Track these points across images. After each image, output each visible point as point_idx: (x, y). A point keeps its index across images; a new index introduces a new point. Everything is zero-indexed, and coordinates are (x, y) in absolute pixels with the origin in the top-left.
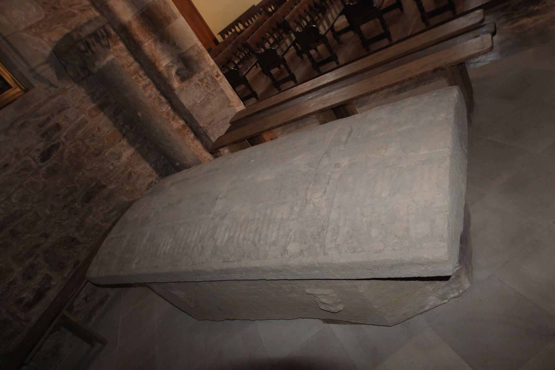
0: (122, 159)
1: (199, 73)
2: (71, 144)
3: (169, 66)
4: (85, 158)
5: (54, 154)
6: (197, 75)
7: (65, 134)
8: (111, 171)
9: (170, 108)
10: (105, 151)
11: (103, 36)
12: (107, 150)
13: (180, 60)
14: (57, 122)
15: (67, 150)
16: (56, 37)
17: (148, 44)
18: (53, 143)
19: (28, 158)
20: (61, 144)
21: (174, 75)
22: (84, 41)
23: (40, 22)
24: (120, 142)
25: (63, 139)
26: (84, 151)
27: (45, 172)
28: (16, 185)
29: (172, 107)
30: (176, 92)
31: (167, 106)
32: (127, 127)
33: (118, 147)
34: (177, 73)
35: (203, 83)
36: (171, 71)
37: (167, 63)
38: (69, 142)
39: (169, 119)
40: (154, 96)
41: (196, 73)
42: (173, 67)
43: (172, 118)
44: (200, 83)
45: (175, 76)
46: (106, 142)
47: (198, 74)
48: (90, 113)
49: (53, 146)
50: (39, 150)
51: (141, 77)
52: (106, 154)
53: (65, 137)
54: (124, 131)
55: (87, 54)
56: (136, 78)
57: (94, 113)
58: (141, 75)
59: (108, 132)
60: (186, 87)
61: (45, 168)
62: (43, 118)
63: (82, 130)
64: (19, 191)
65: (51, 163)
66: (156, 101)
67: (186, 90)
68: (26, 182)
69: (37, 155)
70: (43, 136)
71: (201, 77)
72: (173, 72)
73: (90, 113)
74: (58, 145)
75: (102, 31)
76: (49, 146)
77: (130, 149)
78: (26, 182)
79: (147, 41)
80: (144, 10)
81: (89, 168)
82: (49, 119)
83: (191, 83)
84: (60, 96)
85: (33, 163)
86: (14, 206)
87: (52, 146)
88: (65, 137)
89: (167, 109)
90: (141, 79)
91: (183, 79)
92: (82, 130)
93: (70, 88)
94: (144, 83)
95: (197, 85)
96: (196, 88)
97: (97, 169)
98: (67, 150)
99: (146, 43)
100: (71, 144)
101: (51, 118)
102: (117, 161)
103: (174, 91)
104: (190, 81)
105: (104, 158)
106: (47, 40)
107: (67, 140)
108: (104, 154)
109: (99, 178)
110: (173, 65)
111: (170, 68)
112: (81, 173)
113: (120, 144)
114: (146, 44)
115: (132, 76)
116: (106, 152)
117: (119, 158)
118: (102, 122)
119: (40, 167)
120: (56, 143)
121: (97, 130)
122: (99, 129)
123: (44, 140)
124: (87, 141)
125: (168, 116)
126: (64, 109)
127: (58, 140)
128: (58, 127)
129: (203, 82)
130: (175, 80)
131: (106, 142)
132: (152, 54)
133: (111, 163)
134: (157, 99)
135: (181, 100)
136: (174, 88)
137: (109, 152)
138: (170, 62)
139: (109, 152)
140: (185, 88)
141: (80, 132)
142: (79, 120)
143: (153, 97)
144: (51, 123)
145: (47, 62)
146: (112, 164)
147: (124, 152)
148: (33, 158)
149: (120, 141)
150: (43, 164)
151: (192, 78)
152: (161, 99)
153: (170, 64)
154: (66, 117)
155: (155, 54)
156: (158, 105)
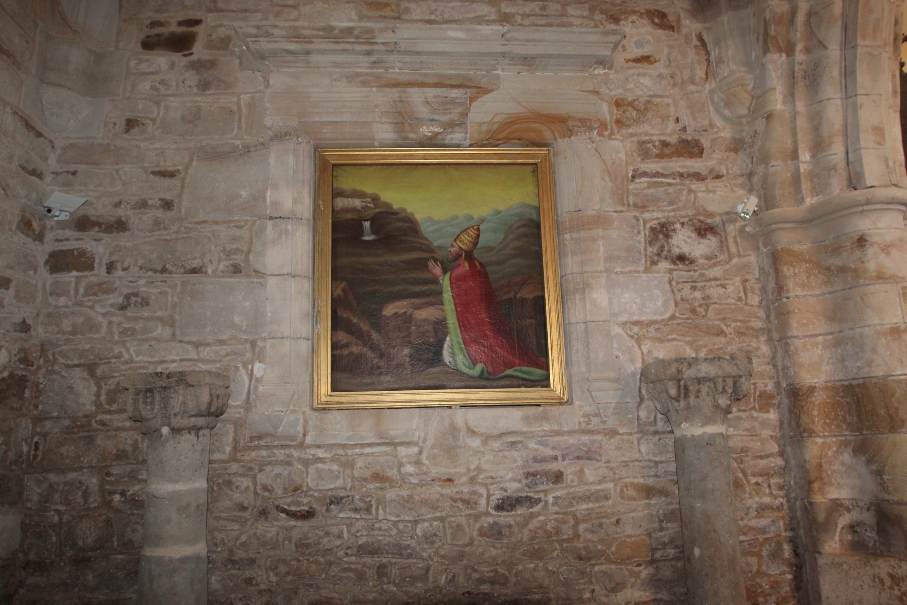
0: (616, 595)
1: (901, 560)
2: (557, 513)
3: (841, 505)
4: (558, 547)
5: (520, 511)
6: (893, 562)
7: (559, 493)
8: (580, 599)
9: (790, 577)
10: (599, 562)
11: (724, 391)
12: (604, 562)
13: (872, 508)
14: (562, 469)
15: (542, 518)
16: (662, 352)
17: (824, 443)
18: (531, 494)
19: (483, 491)
20: (543, 503)
21: (840, 526)
22: (682, 383)
23: (656, 322)
24: (636, 566)
25: (550, 499)
26: (566, 537)
27: (486, 525)
28: (438, 514)
29: (795, 578)
30: (821, 561)
31: (786, 569)
32: (671, 552)
33: (626, 572)
34: (852, 528)
35: (896, 588)
36: (841, 515)
37: (842, 497)
38: (556, 508)
39: (770, 595)
40: (772, 535)
41: (891, 557)
42: (848, 510)
43: (778, 599)
44: (888, 582)
45: (842, 529)
46: (613, 548)
47: (897, 561)
48: (625, 489)
49: (529, 499)
50: (506, 491)
51: (769, 486)
52: (597, 568)
53: (555, 498)
54: (658, 555)
55: (676, 404)
56: (757, 484)
57: (631, 492)
58: (772, 485)
59: (630, 536)
60: (850, 568)
61: (491, 520)
62: (549, 452)
63: (590, 505)
64: (436, 523)
65: (505, 518)
66: (768, 547)
67: (847, 572)
68: (453, 519)
69: (497, 495)
70: (528, 475)
71: (899, 571)
72: (844, 520)
73: (625, 489)
74: (538, 501)
75: (730, 382)
76: (524, 495)
77: (645, 590)
78: (453, 519)
79: (824, 436)
80: (854, 382)
81: (550, 568)
82: (555, 458)
83: (867, 568)
84: (598, 437)
85: (483, 502)
86: (412, 537)
87: (527, 497)
88: (555, 498)
89: (780, 574)
90: (767, 491)
91: (858, 546)
92: (590, 505)
93: (622, 434)
94: (767, 500)
95: (877, 580)
96: (871, 584)
97: (563, 579)
98: (542, 518)
99: (819, 436)
100: (557, 513)
101: (560, 458)
102: (605, 592)
103: (817, 555)
104: (868, 562)
105: (588, 570)
106: (645, 351)
107: (554, 504)
108: (594, 565)
109: (552, 596)
110: (851, 507)
111: (841, 509)
112: (532, 566)
113: (636, 569)
114: (819, 440)
115: (754, 475)
116: (601, 564)
117: (614, 590)
118: (631, 515)
119: (487, 514)
120: (536, 496)
121: (614, 520)
122: (618, 521)
123: (524, 481)
124: (582, 527)
125: (772, 587)
126: (589, 459)
127: (542, 496)
128: (558, 477)
129: (898, 585)
130: (837, 538)
131: (613, 548)
132: (821, 463)
133: (591, 587)
134: (774, 544)
135: (822, 583)
136: (822, 551)
137: (604, 567)
138: (849, 499)
139: (604, 567)
140: (845, 567)
141: (584, 506)
142: (599, 487)
143: (768, 536)
144: (554, 466)
145: (616, 380)
146: (593, 591)
147: (632, 587)
148: (489, 496)
149: (639, 565)
150: (494, 512)
151: (877, 560)
152: (782, 550)
153: (847, 503)
154: (582, 471)
155: (825, 466)
156: (768, 556)
